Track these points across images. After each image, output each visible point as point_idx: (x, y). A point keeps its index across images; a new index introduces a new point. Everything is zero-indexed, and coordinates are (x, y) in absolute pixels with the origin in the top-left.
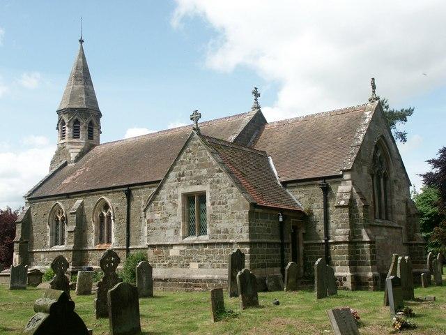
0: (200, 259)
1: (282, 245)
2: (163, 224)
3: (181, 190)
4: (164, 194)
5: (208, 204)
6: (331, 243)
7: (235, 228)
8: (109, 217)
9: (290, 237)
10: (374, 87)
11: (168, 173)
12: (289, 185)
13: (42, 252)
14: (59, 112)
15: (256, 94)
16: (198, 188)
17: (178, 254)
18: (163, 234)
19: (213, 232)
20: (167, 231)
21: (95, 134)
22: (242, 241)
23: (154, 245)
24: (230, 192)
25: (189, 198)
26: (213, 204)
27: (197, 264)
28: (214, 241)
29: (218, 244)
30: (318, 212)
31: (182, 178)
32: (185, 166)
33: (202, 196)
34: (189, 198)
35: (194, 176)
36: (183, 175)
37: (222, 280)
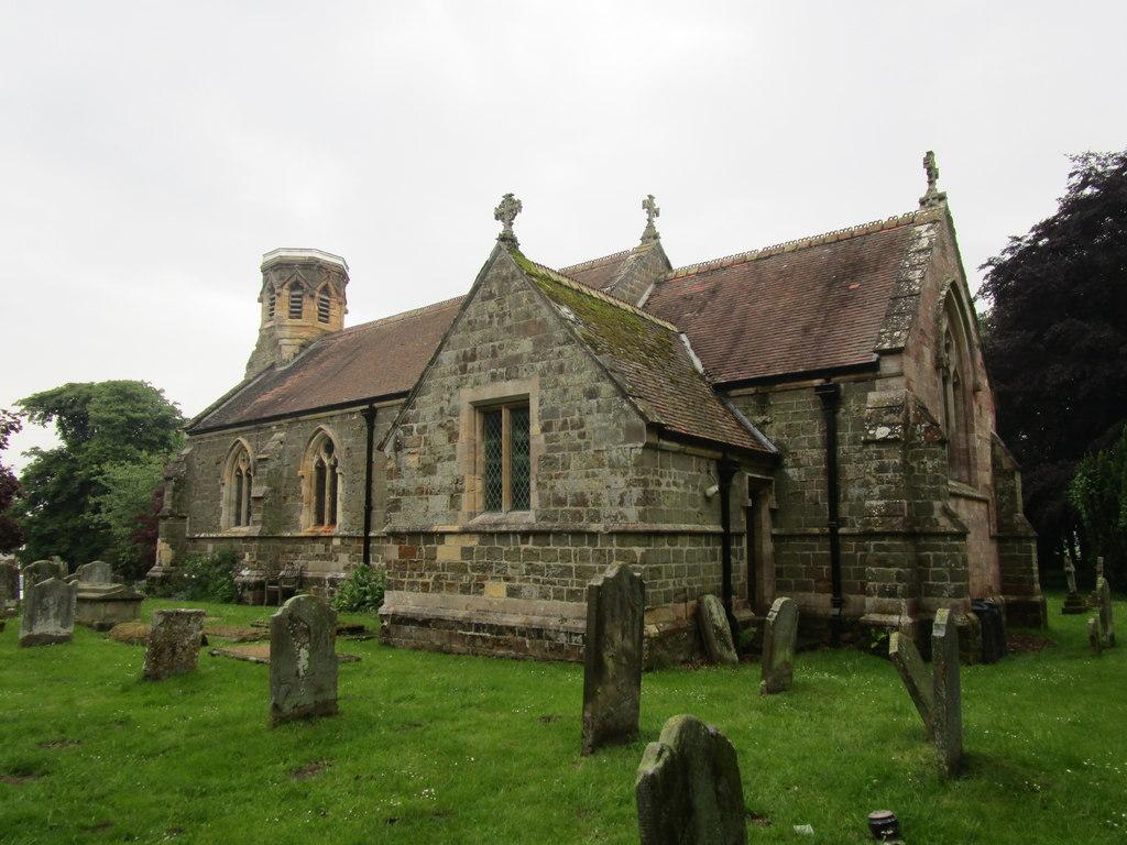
0: (510, 572)
1: (726, 538)
2: (423, 481)
3: (467, 395)
5: (535, 428)
6: (844, 535)
7: (605, 492)
9: (744, 519)
10: (932, 174)
11: (438, 352)
12: (734, 393)
13: (212, 538)
14: (268, 269)
15: (650, 206)
16: (509, 389)
17: (457, 558)
19: (545, 502)
25: (489, 412)
27: (504, 585)
28: (548, 525)
29: (559, 534)
30: (811, 454)
31: (470, 365)
32: (478, 335)
33: (520, 407)
34: (489, 412)
35: (501, 356)
36: (473, 358)
37: (570, 634)
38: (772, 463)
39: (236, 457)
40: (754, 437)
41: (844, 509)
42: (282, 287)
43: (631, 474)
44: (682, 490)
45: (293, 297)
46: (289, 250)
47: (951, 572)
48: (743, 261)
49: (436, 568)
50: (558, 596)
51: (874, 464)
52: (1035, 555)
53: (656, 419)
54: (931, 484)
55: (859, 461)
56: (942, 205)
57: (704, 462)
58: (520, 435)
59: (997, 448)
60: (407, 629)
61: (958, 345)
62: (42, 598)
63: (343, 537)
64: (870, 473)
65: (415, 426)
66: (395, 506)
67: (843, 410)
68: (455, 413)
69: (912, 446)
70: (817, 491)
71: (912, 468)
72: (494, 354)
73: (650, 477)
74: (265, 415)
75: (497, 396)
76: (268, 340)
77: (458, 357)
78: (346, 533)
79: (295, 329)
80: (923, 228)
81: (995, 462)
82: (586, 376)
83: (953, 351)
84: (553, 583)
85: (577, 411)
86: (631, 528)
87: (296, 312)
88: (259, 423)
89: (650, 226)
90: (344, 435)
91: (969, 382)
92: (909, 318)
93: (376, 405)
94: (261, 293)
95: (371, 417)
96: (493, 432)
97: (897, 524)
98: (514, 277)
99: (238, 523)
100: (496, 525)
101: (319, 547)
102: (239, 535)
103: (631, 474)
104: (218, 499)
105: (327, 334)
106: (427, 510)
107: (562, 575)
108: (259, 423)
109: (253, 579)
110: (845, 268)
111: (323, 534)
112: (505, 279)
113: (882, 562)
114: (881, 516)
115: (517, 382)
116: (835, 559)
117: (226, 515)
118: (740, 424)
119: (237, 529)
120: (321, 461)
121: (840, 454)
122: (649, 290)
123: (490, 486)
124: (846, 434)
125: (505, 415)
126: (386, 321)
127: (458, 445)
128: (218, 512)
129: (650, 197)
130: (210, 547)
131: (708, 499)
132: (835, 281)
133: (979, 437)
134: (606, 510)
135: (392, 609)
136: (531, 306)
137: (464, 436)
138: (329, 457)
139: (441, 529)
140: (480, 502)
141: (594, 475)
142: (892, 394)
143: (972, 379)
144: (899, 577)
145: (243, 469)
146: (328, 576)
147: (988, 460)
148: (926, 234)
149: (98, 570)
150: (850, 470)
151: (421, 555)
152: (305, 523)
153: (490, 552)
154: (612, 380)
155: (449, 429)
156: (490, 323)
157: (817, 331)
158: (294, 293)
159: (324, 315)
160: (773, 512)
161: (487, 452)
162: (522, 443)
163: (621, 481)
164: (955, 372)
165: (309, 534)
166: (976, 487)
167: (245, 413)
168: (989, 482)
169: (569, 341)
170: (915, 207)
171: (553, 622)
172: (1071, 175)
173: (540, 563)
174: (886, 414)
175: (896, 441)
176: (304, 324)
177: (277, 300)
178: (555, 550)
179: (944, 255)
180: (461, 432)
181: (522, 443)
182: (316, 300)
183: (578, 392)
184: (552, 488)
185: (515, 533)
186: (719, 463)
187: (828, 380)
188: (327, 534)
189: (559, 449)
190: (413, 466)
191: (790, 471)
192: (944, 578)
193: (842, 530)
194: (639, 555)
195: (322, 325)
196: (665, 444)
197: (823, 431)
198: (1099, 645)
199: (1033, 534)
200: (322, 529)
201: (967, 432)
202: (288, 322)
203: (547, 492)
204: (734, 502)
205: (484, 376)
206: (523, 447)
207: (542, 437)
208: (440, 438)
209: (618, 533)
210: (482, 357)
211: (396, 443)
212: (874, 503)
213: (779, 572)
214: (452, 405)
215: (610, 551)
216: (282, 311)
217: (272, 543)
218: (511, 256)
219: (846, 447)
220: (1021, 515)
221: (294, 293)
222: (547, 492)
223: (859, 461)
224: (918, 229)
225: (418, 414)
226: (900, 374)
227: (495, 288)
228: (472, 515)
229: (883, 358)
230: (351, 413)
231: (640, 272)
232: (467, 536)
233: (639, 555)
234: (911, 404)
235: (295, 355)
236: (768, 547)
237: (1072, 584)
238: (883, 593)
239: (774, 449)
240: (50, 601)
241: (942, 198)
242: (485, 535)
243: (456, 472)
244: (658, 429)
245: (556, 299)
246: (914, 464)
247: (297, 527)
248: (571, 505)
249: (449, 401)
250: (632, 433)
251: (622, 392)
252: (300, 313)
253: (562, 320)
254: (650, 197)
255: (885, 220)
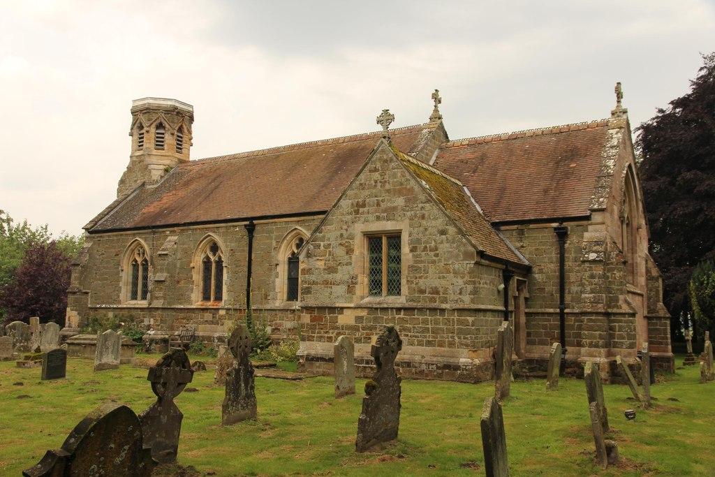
2: (330, 277)
3: (359, 228)
4: (331, 232)
5: (405, 249)
6: (568, 314)
8: (219, 263)
10: (619, 96)
12: (503, 228)
14: (134, 112)
15: (436, 98)
16: (389, 226)
17: (352, 322)
18: (327, 291)
20: (335, 288)
21: (184, 145)
22: (461, 306)
23: (311, 308)
24: (443, 232)
25: (374, 240)
26: (413, 250)
28: (414, 305)
29: (420, 310)
31: (361, 210)
32: (367, 192)
33: (395, 238)
34: (374, 240)
35: (383, 206)
36: (364, 205)
38: (527, 270)
39: (133, 250)
40: (516, 255)
41: (568, 298)
42: (150, 126)
43: (467, 278)
44: (488, 286)
45: (158, 133)
46: (155, 99)
47: (628, 334)
48: (499, 139)
49: (337, 328)
50: (420, 344)
51: (587, 274)
52: (669, 328)
53: (481, 248)
54: (618, 285)
55: (578, 271)
56: (625, 117)
57: (497, 270)
58: (393, 253)
59: (649, 263)
60: (317, 364)
61: (630, 201)
62: (106, 341)
63: (228, 310)
64: (585, 279)
65: (322, 244)
66: (307, 291)
67: (569, 242)
68: (351, 237)
69: (608, 264)
70: (552, 288)
71: (608, 277)
72: (378, 205)
73: (477, 279)
74: (158, 223)
75: (380, 229)
76: (137, 165)
77: (352, 204)
78: (230, 307)
79: (160, 157)
80: (613, 131)
81: (648, 271)
82: (440, 222)
83: (627, 205)
84: (416, 337)
85: (433, 242)
86: (466, 307)
87: (160, 144)
88: (152, 227)
89: (436, 110)
90: (229, 243)
91: (635, 224)
92: (608, 190)
93: (255, 222)
94: (132, 129)
95: (251, 229)
96: (375, 249)
97: (601, 308)
98: (391, 160)
99: (134, 297)
100: (379, 303)
101: (208, 316)
102: (137, 306)
103: (467, 278)
104: (118, 280)
105: (181, 162)
106: (331, 293)
107: (423, 332)
108: (152, 227)
109: (159, 337)
110: (566, 152)
111: (210, 307)
112: (386, 161)
113: (590, 328)
114: (591, 302)
115: (394, 222)
116: (562, 327)
117: (125, 292)
118: (509, 249)
119: (134, 302)
120: (208, 258)
121: (566, 268)
122: (436, 153)
123: (373, 281)
124: (570, 256)
125: (384, 241)
126: (234, 157)
127: (353, 257)
128: (119, 290)
129: (436, 90)
130: (111, 315)
131: (499, 292)
132: (560, 160)
133: (640, 257)
134: (452, 297)
135: (306, 353)
136: (403, 179)
137: (357, 252)
138: (214, 255)
139: (341, 305)
140: (367, 290)
141: (444, 277)
142: (597, 234)
143: (636, 221)
144: (601, 337)
145: (139, 260)
146: (216, 335)
147: (644, 270)
148: (616, 136)
149: (52, 329)
150: (572, 277)
151: (326, 321)
152: (196, 300)
153: (376, 319)
154: (456, 226)
155: (347, 247)
156: (375, 186)
157: (552, 193)
158: (158, 131)
159: (179, 148)
160: (526, 299)
161: (371, 261)
162: (394, 257)
163: (460, 281)
164: (628, 217)
165: (200, 307)
166: (637, 286)
167: (136, 220)
168: (643, 284)
169: (428, 201)
170: (608, 116)
171: (417, 358)
172: (701, 69)
173: (408, 326)
174: (595, 246)
175: (600, 261)
176: (167, 154)
177: (146, 135)
178: (418, 318)
179: (625, 148)
180: (356, 248)
181: (394, 257)
182: (175, 136)
183: (435, 230)
184: (417, 284)
185: (392, 308)
186: (504, 271)
187: (561, 224)
188: (215, 307)
189: (422, 262)
190: (321, 267)
191: (536, 276)
192: (623, 338)
193: (566, 311)
194: (470, 322)
195: (178, 155)
196: (483, 261)
197: (557, 254)
198: (704, 378)
199: (668, 315)
200: (209, 303)
201: (633, 253)
202: (155, 152)
203: (414, 286)
204: (510, 293)
205: (371, 217)
206: (398, 260)
207: (411, 255)
208: (340, 252)
209: (459, 310)
210: (370, 206)
211: (308, 253)
212: (587, 295)
213: (529, 334)
214: (349, 232)
215: (453, 319)
216: (149, 142)
217: (169, 312)
218: (390, 148)
219: (570, 263)
220: (661, 304)
221: (158, 131)
222: (414, 286)
223: (578, 271)
224: (611, 131)
225: (324, 237)
226: (603, 223)
227: (378, 165)
228: (362, 298)
229: (593, 213)
230: (233, 226)
231: (431, 141)
232: (360, 310)
233: (470, 322)
234: (608, 240)
235: (162, 177)
236: (523, 319)
237: (690, 348)
238: (591, 345)
239: (527, 263)
240: (109, 343)
241: (625, 112)
242: (372, 309)
243: (351, 273)
244: (481, 254)
245: (418, 176)
246: (609, 274)
247: (189, 301)
248: (429, 293)
249: (347, 230)
250: (467, 256)
251: (460, 231)
252: (162, 146)
253: (424, 189)
254: (436, 90)
255: (589, 122)
